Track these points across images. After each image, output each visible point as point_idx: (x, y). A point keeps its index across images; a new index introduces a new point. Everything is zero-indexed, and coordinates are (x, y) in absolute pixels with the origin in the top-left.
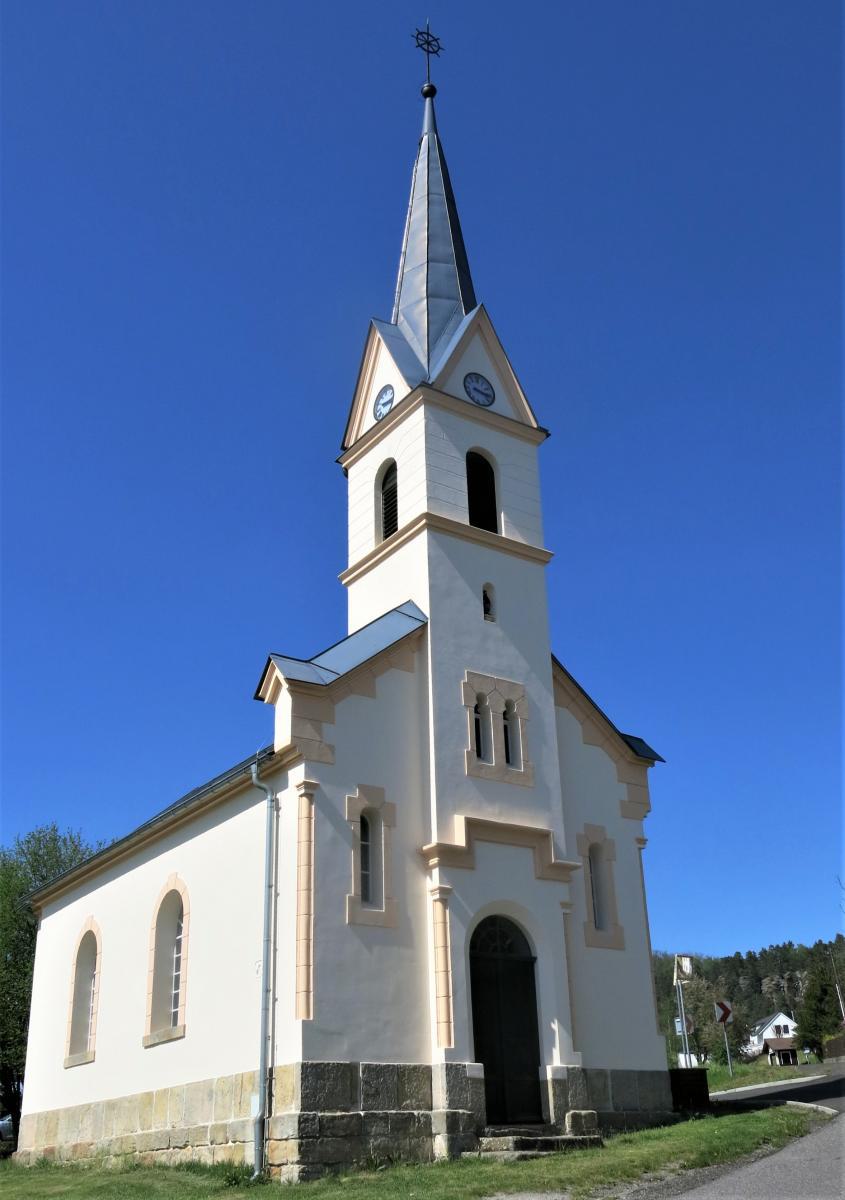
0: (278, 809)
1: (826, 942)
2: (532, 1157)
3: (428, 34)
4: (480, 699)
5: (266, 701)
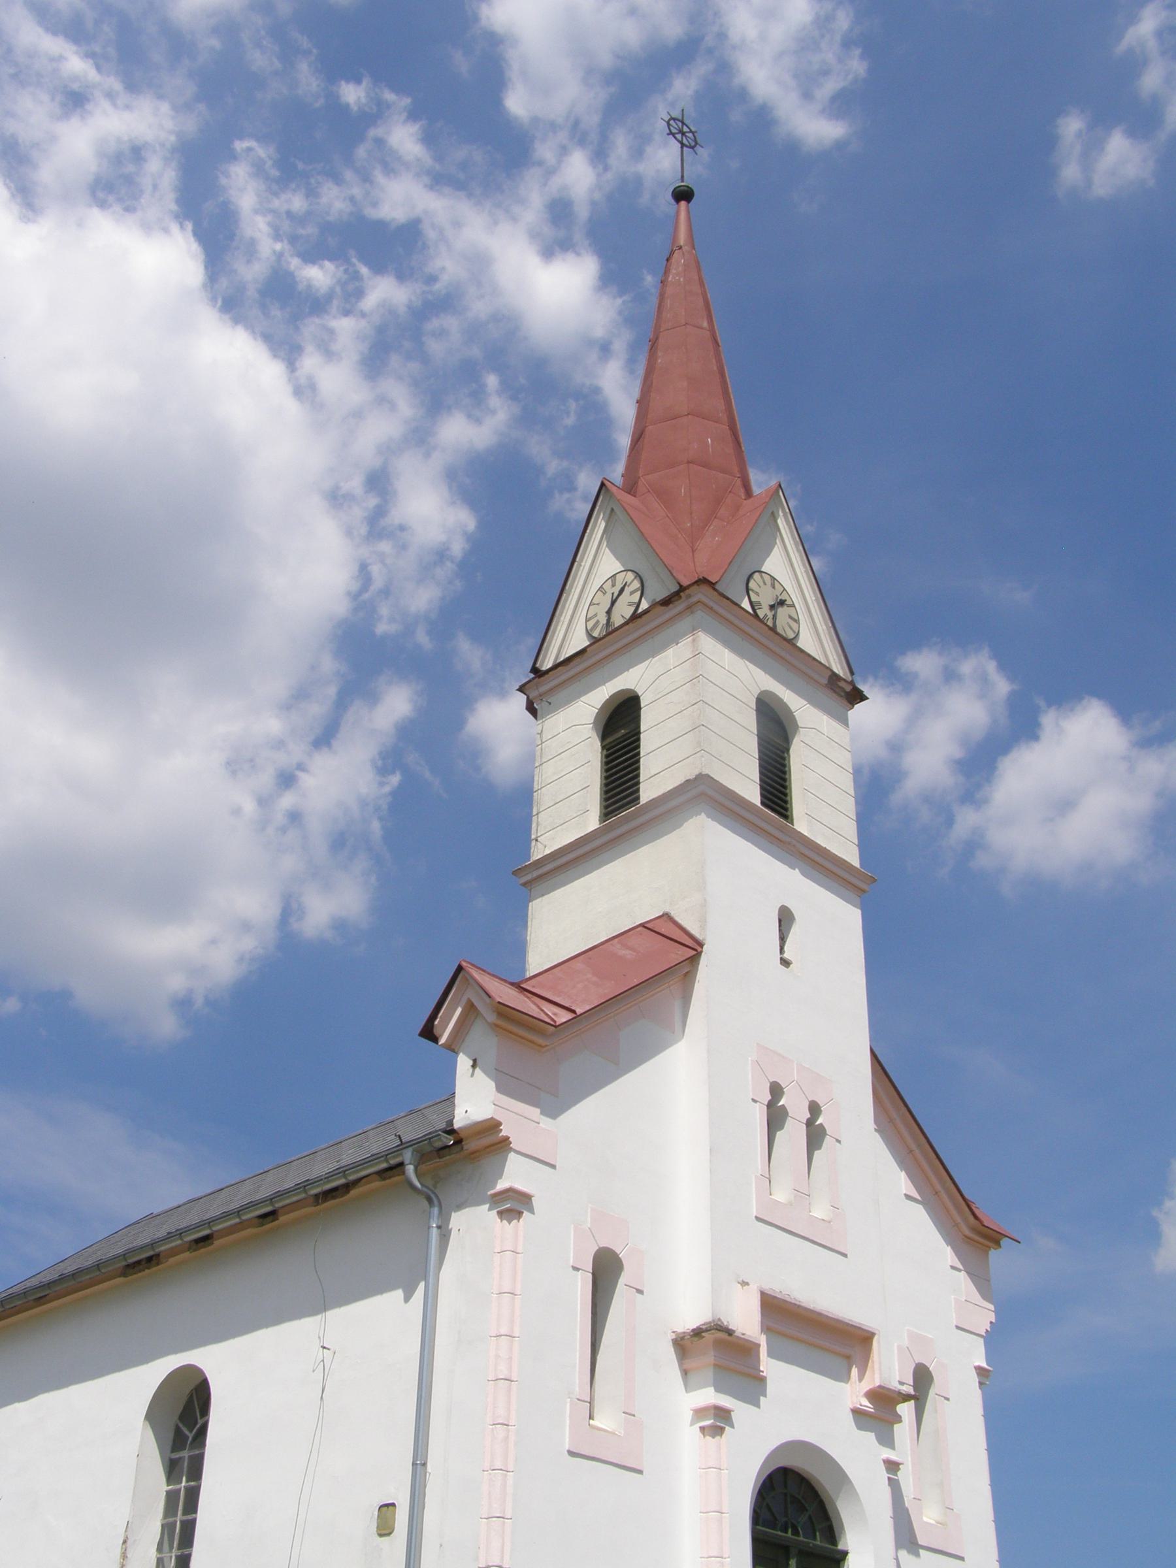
3: (683, 123)
4: (776, 1090)
5: (442, 1041)
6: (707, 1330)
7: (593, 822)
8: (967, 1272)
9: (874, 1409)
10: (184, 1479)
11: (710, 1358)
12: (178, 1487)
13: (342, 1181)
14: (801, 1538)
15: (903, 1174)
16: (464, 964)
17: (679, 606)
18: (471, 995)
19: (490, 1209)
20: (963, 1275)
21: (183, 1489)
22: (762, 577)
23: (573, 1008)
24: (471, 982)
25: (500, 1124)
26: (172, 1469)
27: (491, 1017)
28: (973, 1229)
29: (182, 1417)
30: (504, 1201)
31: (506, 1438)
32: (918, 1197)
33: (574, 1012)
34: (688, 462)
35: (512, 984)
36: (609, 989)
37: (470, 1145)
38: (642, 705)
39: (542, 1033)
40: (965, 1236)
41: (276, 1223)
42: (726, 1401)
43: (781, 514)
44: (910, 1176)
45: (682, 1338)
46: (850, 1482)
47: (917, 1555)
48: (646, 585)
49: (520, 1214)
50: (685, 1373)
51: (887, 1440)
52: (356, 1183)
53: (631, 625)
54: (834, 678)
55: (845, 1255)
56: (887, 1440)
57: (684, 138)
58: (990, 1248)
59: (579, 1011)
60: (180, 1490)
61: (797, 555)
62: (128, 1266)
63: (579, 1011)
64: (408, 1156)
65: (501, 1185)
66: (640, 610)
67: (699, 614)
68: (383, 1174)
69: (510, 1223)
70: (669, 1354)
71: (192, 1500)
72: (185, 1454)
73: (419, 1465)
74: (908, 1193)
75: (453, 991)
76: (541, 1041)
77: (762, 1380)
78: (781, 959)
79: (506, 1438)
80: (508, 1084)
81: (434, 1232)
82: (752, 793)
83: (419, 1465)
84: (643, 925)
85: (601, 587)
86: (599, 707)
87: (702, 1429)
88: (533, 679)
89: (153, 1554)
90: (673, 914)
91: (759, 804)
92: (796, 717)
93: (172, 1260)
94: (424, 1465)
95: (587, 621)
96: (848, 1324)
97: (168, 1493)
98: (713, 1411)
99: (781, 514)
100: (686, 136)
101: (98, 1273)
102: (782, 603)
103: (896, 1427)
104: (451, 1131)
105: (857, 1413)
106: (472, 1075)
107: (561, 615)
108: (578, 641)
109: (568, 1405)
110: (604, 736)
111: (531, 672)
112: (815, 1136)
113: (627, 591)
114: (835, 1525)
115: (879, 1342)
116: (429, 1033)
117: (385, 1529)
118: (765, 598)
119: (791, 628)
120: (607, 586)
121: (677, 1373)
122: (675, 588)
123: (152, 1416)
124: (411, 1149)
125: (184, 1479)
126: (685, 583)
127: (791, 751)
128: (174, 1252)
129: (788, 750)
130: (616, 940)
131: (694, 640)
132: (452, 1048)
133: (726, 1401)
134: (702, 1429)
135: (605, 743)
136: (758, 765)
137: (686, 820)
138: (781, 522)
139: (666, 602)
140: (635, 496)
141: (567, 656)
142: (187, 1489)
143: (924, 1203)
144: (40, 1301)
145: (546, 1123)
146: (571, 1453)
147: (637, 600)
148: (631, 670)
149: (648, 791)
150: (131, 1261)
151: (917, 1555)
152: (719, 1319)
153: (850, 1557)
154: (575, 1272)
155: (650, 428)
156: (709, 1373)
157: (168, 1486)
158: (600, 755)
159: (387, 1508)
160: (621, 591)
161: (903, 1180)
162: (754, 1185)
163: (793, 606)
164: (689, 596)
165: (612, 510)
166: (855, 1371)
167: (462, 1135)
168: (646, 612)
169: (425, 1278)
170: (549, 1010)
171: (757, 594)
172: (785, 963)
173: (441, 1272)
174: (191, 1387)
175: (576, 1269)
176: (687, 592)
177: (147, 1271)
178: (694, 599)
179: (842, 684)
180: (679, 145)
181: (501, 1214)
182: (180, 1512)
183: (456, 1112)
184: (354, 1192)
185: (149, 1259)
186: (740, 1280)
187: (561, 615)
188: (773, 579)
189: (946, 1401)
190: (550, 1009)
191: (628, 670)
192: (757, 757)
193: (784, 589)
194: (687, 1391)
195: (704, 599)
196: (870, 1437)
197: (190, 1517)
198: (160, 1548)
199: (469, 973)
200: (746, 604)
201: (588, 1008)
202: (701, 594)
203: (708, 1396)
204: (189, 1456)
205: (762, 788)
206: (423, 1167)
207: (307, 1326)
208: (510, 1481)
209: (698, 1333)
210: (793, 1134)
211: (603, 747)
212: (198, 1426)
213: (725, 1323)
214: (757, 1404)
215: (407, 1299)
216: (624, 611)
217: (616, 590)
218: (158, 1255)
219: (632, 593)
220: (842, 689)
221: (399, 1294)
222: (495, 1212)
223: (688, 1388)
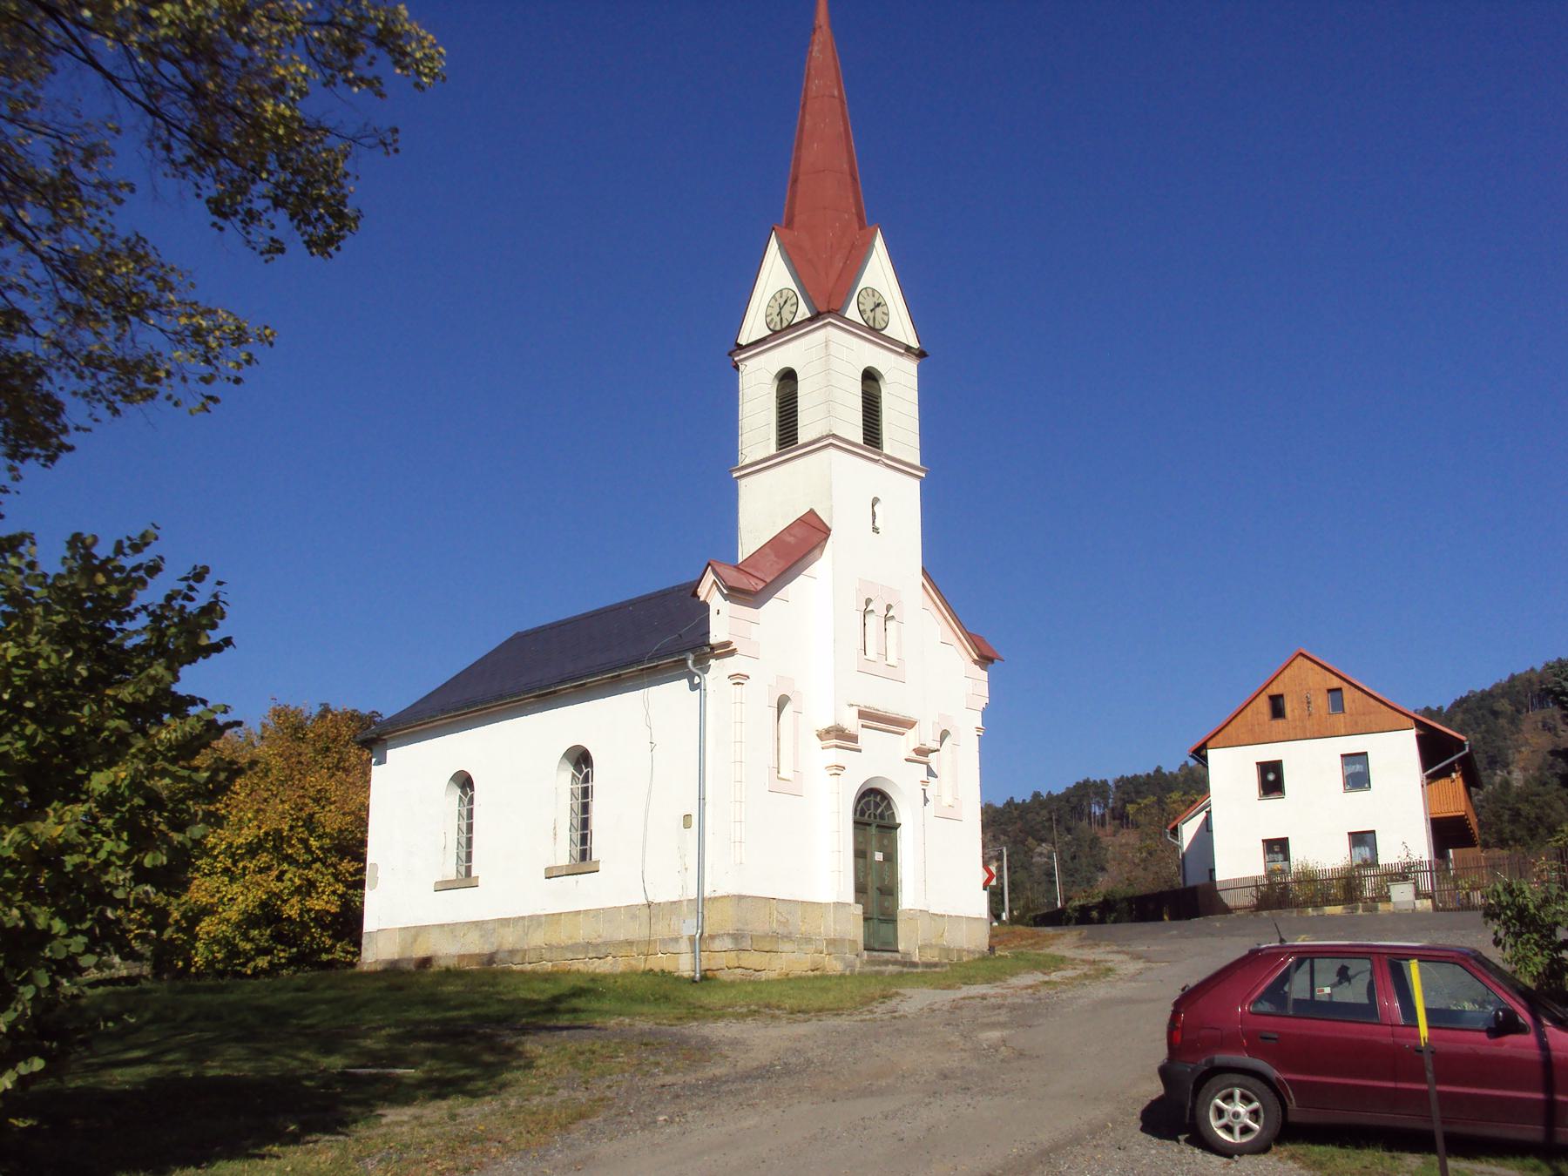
1: (1018, 800)
9: (926, 471)
59: (768, 581)
63: (768, 581)
73: (702, 799)
82: (857, 435)
83: (702, 799)
91: (862, 443)
102: (879, 305)
113: (789, 303)
117: (687, 825)
120: (778, 296)
126: (821, 310)
149: (804, 435)
159: (687, 817)
160: (785, 302)
171: (863, 304)
172: (875, 530)
188: (873, 290)
190: (753, 581)
219: (792, 305)
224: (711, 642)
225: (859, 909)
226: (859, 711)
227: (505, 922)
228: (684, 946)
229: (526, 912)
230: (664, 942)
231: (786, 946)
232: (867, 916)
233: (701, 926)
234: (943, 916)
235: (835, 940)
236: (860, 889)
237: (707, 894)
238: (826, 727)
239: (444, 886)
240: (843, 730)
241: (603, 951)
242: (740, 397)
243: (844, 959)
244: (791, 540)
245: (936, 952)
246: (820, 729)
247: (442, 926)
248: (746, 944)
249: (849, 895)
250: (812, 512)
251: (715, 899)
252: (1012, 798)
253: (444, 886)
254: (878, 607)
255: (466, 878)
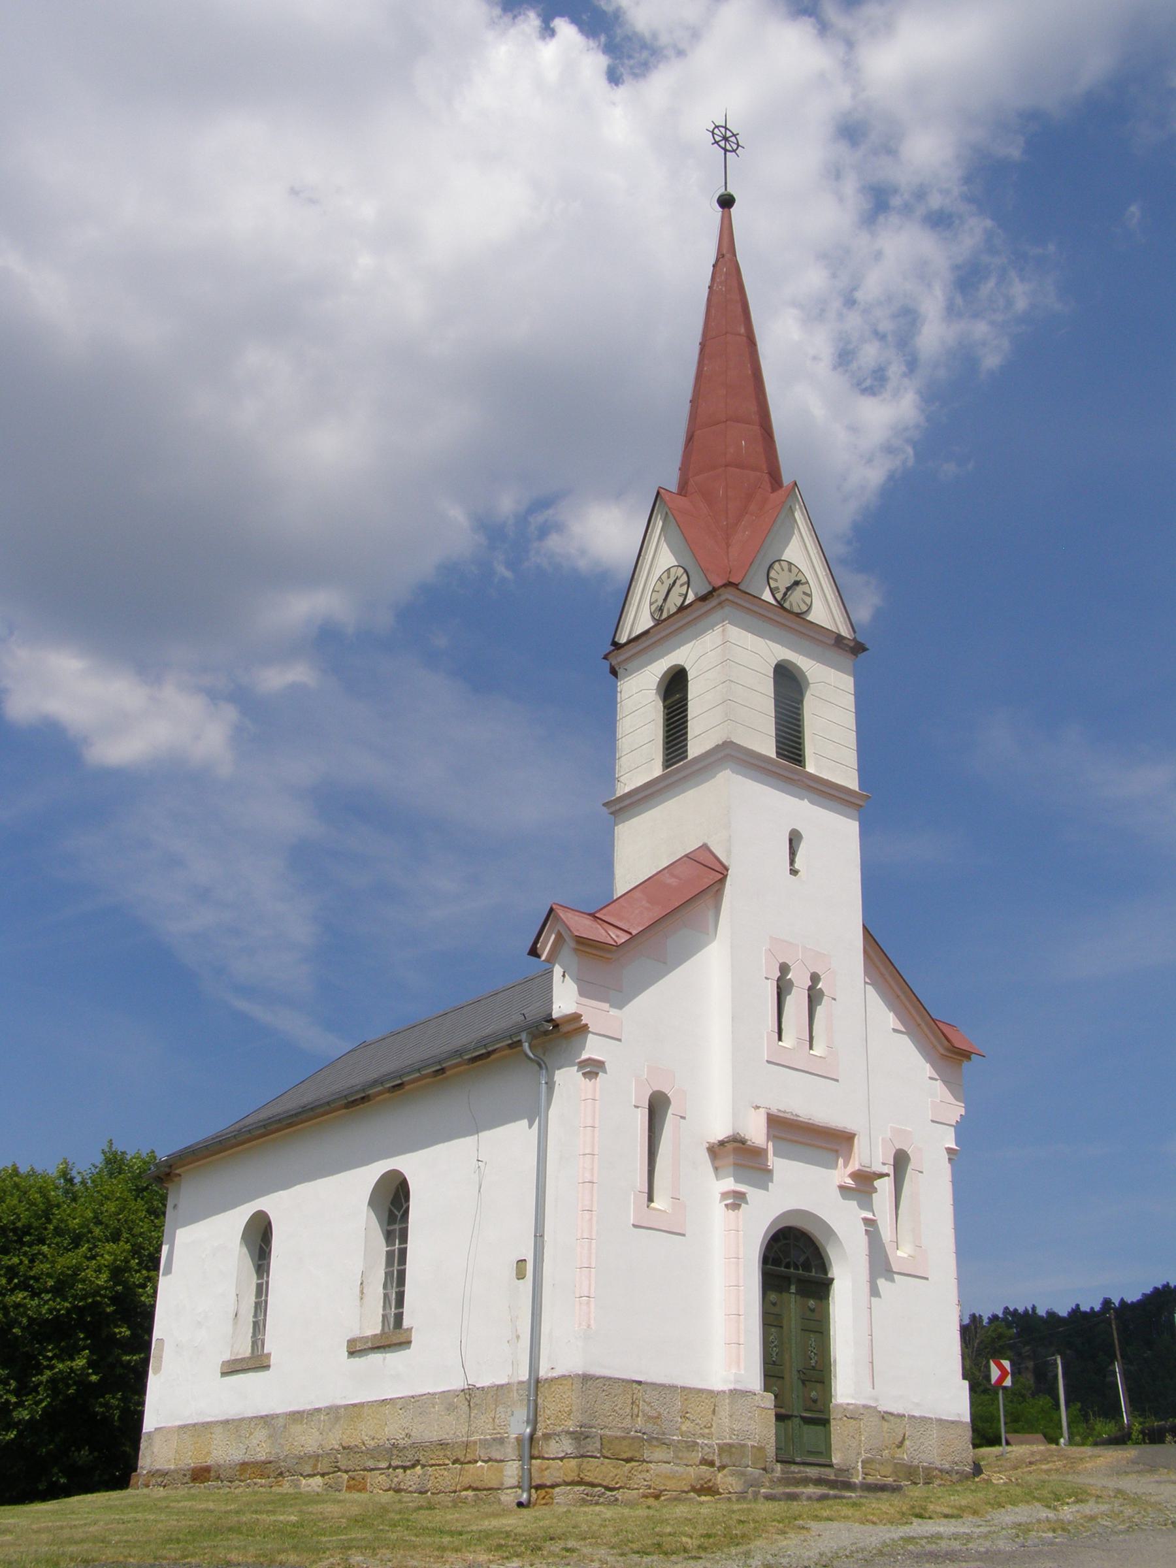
0: (207, 1469)
1: (1085, 1308)
2: (836, 1497)
3: (726, 129)
4: (784, 969)
5: (543, 958)
6: (727, 1142)
7: (657, 770)
8: (942, 1081)
10: (397, 1241)
11: (731, 1159)
12: (393, 1248)
13: (484, 1051)
14: (801, 1272)
15: (891, 1014)
16: (554, 907)
17: (713, 602)
18: (559, 927)
19: (578, 1071)
20: (939, 1082)
21: (396, 1250)
22: (780, 565)
23: (630, 931)
24: (558, 918)
25: (581, 1016)
26: (389, 1236)
27: (572, 944)
28: (948, 1050)
29: (393, 1203)
30: (587, 1065)
31: (591, 1220)
32: (904, 1030)
33: (630, 933)
34: (726, 466)
35: (589, 914)
36: (657, 913)
37: (564, 1029)
38: (689, 679)
39: (609, 951)
40: (943, 1055)
41: (444, 1075)
42: (741, 1188)
43: (797, 507)
44: (897, 1014)
45: (713, 1147)
46: (835, 1234)
47: (893, 1280)
48: (691, 579)
49: (597, 1074)
50: (716, 1169)
51: (867, 1204)
52: (494, 1051)
53: (679, 614)
54: (839, 639)
55: (837, 1080)
56: (867, 1204)
57: (727, 144)
58: (963, 1061)
59: (634, 932)
60: (394, 1250)
61: (810, 539)
62: (349, 1103)
63: (634, 932)
64: (524, 1036)
65: (584, 1056)
66: (686, 603)
67: (727, 609)
68: (510, 1046)
69: (590, 1080)
70: (706, 1157)
71: (403, 1253)
72: (397, 1227)
73: (539, 1236)
74: (896, 1028)
75: (548, 924)
76: (608, 956)
77: (768, 1172)
78: (791, 870)
79: (591, 1220)
80: (587, 990)
81: (544, 1087)
82: (768, 747)
83: (539, 1236)
84: (686, 856)
85: (660, 577)
86: (655, 687)
87: (726, 1205)
88: (613, 651)
89: (381, 1290)
90: (709, 844)
91: (774, 755)
92: (808, 677)
93: (378, 1098)
94: (542, 1236)
95: (651, 604)
96: (834, 1129)
97: (387, 1252)
98: (732, 1194)
99: (797, 507)
100: (729, 141)
101: (328, 1107)
102: (797, 583)
103: (874, 1195)
104: (550, 1020)
105: (842, 1188)
106: (563, 982)
107: (632, 598)
108: (645, 622)
109: (632, 1196)
110: (665, 699)
111: (612, 645)
112: (814, 997)
113: (678, 583)
114: (826, 1261)
115: (859, 1139)
116: (534, 952)
117: (521, 1275)
118: (782, 580)
119: (805, 602)
120: (665, 577)
121: (711, 1169)
122: (710, 589)
123: (373, 1202)
124: (525, 1032)
125: (397, 1241)
127: (805, 702)
128: (379, 1094)
129: (802, 701)
130: (666, 871)
131: (723, 630)
132: (551, 960)
133: (741, 1188)
134: (726, 1205)
135: (666, 704)
136: (774, 722)
137: (719, 772)
138: (798, 515)
139: (703, 599)
140: (685, 496)
141: (637, 633)
142: (400, 1250)
143: (908, 1033)
144: (290, 1125)
145: (614, 1012)
146: (635, 1226)
147: (684, 592)
148: (682, 648)
149: (696, 747)
150: (350, 1100)
151: (893, 1280)
152: (738, 1133)
153: (835, 1282)
154: (636, 1109)
155: (698, 433)
156: (731, 1169)
157: (387, 1247)
158: (662, 713)
160: (675, 582)
161: (891, 1020)
162: (765, 1038)
163: (807, 582)
164: (719, 595)
165: (667, 513)
166: (841, 1161)
167: (558, 1022)
168: (690, 605)
169: (539, 1114)
170: (614, 933)
171: (776, 580)
172: (794, 872)
173: (550, 1110)
174: (398, 1183)
175: (637, 1107)
176: (717, 592)
177: (362, 1106)
178: (723, 598)
179: (845, 642)
180: (723, 151)
181: (584, 1074)
182: (396, 1264)
183: (554, 1007)
184: (493, 1057)
185: (363, 1098)
186: (754, 1105)
187: (646, 554)
188: (790, 564)
189: (920, 1174)
190: (613, 933)
191: (679, 648)
192: (774, 716)
193: (800, 570)
194: (717, 1180)
195: (730, 597)
196: (853, 1204)
197: (402, 1267)
198: (385, 1286)
199: (557, 913)
200: (767, 596)
201: (641, 929)
202: (728, 594)
203: (729, 1184)
204: (400, 1229)
205: (777, 741)
206: (535, 1042)
207: (468, 1142)
208: (594, 1246)
209: (722, 1143)
210: (796, 1002)
211: (665, 707)
212: (404, 1208)
213: (743, 1135)
214: (767, 1189)
215: (530, 1126)
216: (675, 601)
217: (671, 581)
218: (368, 1096)
219: (682, 585)
220: (847, 645)
221: (525, 1122)
222: (580, 1073)
223: (718, 1178)
224: (554, 1016)
225: (769, 1400)
226: (768, 1114)
227: (297, 1417)
228: (510, 1451)
229: (322, 1402)
230: (484, 1443)
231: (659, 1454)
232: (783, 1411)
233: (534, 1422)
234: (902, 1416)
235: (730, 1446)
236: (772, 1373)
237: (543, 1373)
238: (720, 1138)
239: (232, 1368)
240: (743, 1142)
241: (410, 1457)
242: (618, 710)
243: (743, 1474)
244: (672, 881)
245: (888, 1470)
246: (712, 1141)
247: (226, 1422)
248: (593, 1447)
249: (752, 1377)
250: (705, 847)
251: (553, 1380)
252: (1078, 1306)
253: (232, 1368)
254: (800, 979)
255: (257, 1362)
